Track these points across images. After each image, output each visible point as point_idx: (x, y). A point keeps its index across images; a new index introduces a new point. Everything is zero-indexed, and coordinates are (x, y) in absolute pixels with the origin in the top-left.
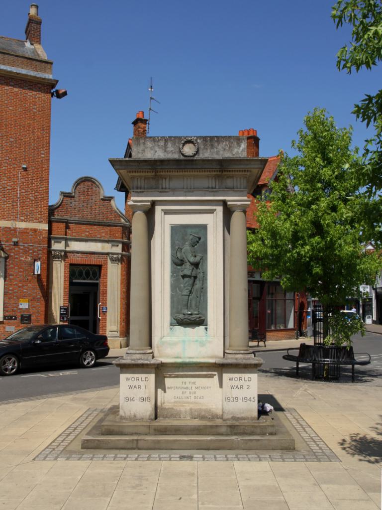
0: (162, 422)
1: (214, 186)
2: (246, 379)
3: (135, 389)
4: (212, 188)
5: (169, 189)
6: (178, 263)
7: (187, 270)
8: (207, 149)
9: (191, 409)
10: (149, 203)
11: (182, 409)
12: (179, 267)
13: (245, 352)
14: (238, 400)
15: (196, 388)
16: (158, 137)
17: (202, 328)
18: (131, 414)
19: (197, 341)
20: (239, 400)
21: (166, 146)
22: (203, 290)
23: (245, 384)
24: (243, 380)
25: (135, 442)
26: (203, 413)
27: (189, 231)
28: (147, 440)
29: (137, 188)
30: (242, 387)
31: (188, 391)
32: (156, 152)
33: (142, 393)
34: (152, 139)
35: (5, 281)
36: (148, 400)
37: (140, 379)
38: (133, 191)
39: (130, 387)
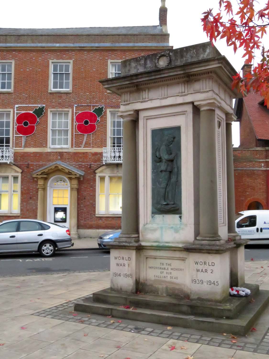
0: (141, 297)
1: (183, 91)
2: (210, 264)
3: (202, 272)
4: (182, 93)
5: (148, 98)
6: (157, 159)
7: (163, 166)
8: (177, 60)
9: (167, 288)
10: (132, 113)
11: (160, 287)
12: (158, 164)
13: (211, 239)
14: (203, 282)
15: (172, 269)
16: (140, 57)
17: (177, 216)
18: (118, 286)
19: (172, 228)
20: (204, 282)
21: (145, 64)
22: (178, 184)
23: (209, 268)
24: (207, 264)
25: (110, 310)
26: (177, 292)
27: (166, 132)
28: (119, 310)
29: (125, 102)
30: (206, 271)
31: (165, 271)
32: (138, 69)
33: (126, 270)
34: (135, 60)
35: (78, 195)
36: (131, 277)
37: (125, 259)
38: (122, 105)
39: (118, 265)
